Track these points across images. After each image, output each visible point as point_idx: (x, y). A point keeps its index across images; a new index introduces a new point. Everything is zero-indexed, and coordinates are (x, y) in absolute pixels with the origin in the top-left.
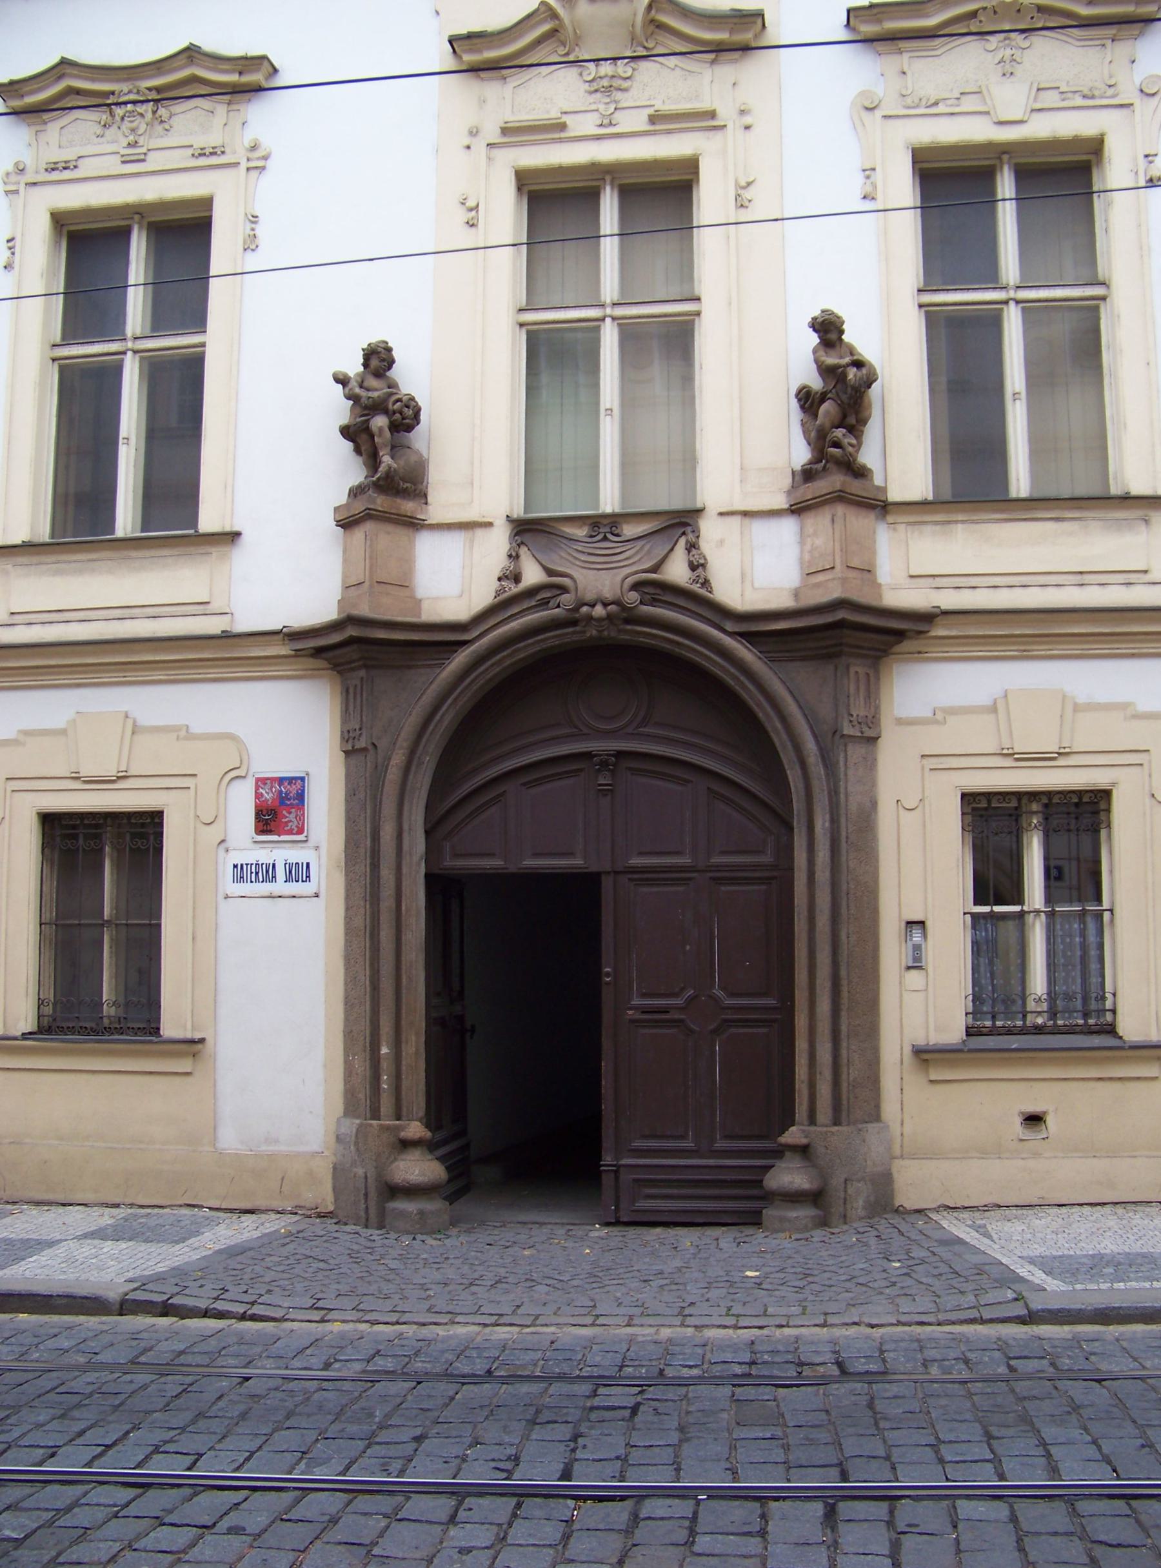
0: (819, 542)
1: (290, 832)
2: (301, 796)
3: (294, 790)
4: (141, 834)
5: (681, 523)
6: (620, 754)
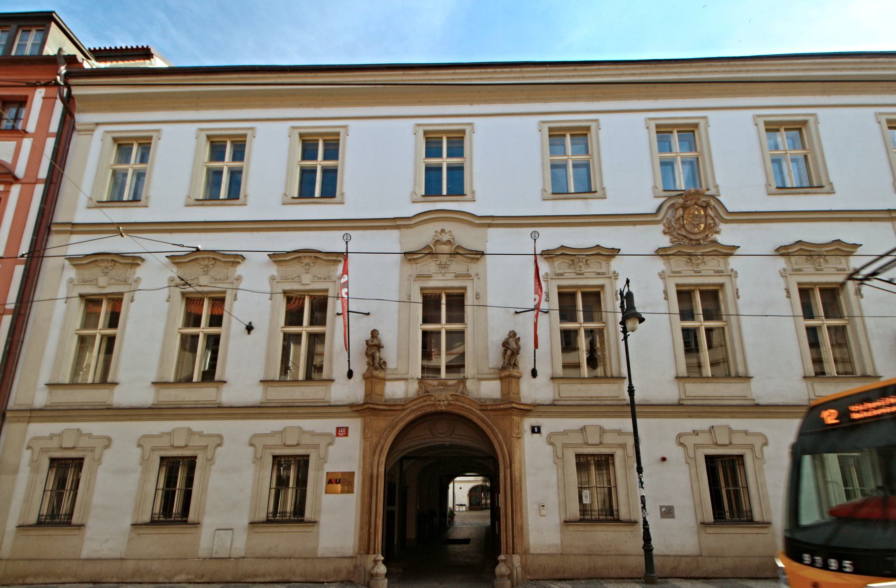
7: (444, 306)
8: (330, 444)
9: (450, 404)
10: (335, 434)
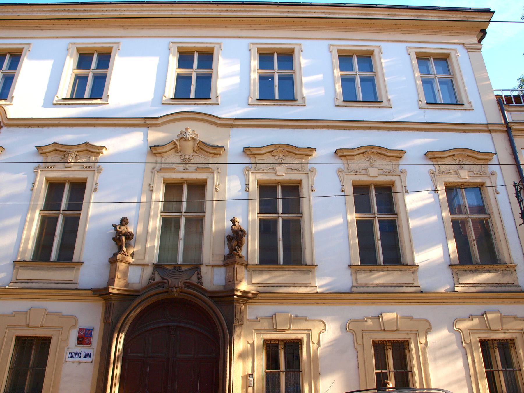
0: (230, 274)
1: (87, 344)
2: (91, 334)
3: (89, 332)
4: (44, 343)
5: (196, 267)
6: (177, 326)
7: (187, 197)
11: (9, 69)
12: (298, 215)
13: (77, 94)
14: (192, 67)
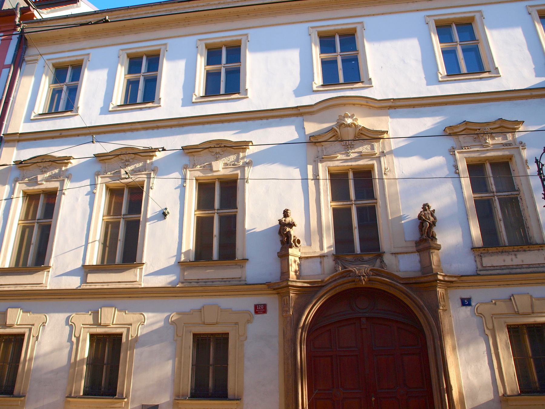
4: (222, 340)
8: (249, 321)
9: (370, 280)
10: (253, 312)
11: (72, 81)
12: (349, 203)
13: (130, 100)
14: (220, 63)
